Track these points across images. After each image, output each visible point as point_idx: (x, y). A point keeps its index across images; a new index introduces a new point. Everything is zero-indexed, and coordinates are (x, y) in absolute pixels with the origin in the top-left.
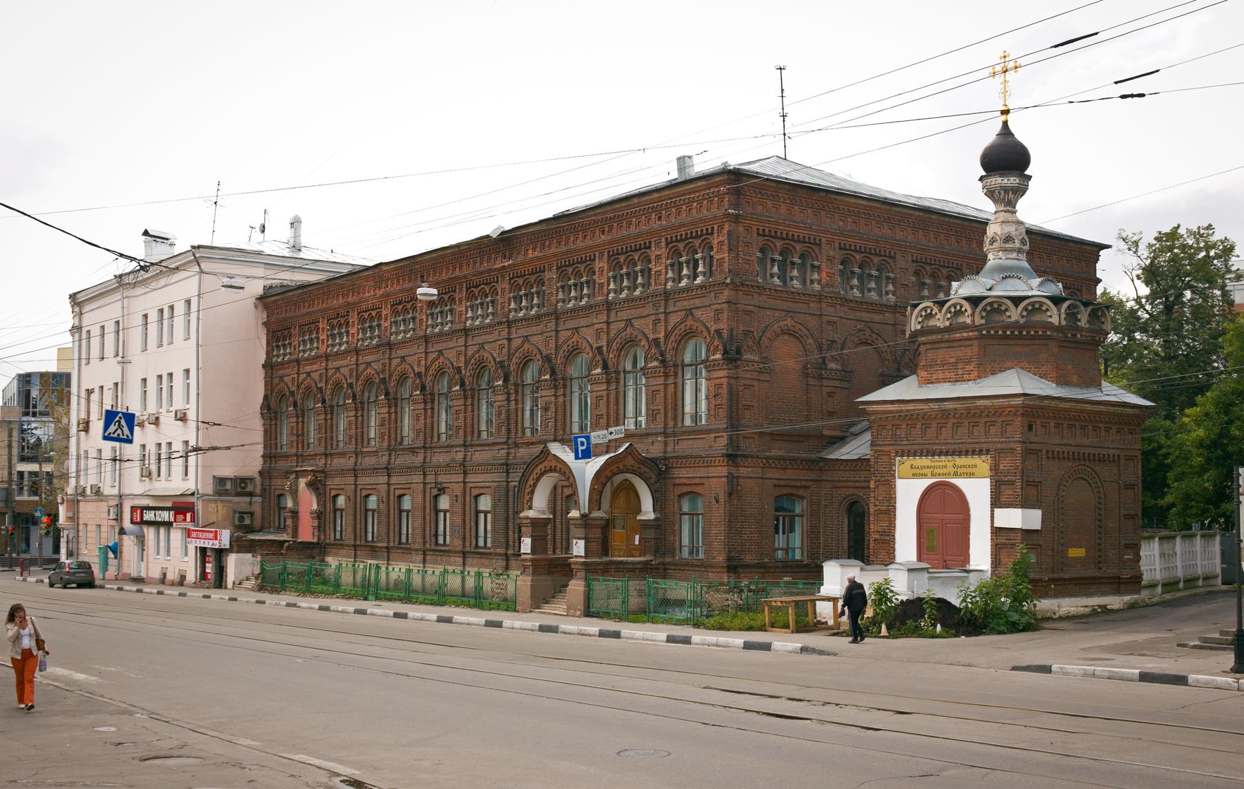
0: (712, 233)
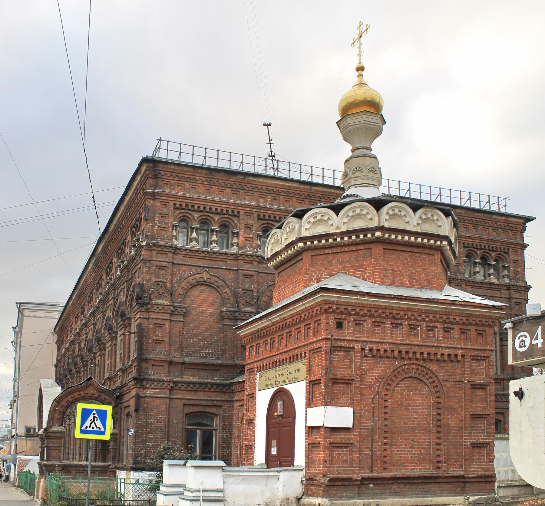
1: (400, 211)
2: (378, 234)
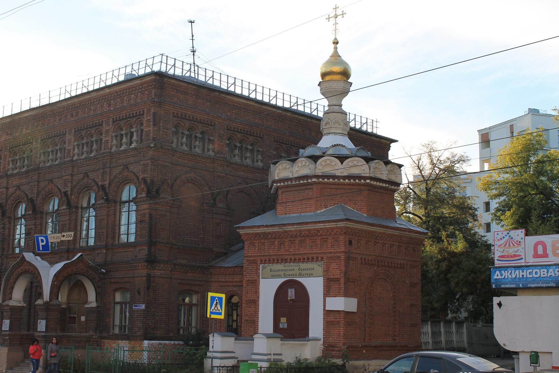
0: (143, 114)
2: (368, 181)
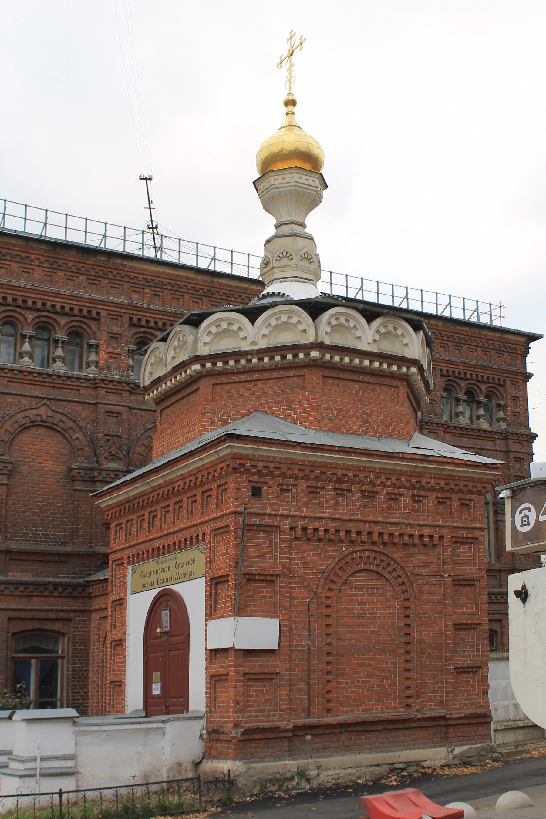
1: (348, 321)
2: (315, 354)
